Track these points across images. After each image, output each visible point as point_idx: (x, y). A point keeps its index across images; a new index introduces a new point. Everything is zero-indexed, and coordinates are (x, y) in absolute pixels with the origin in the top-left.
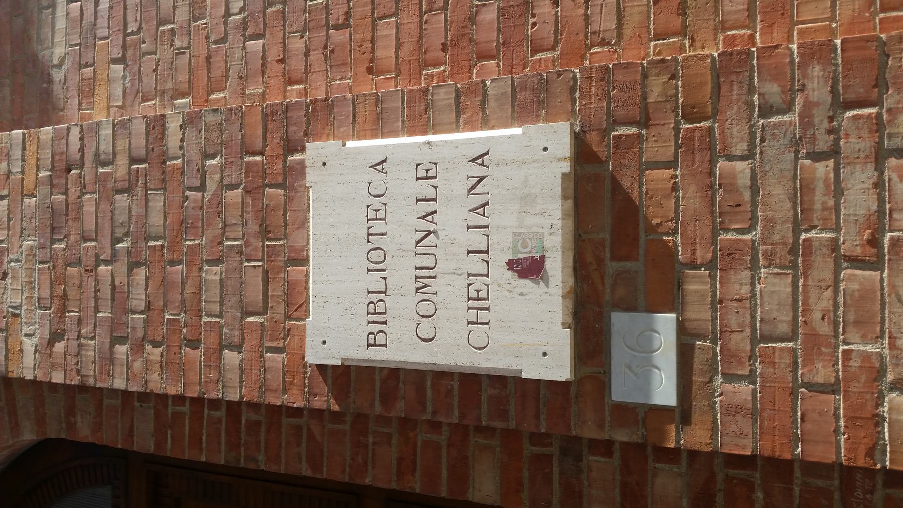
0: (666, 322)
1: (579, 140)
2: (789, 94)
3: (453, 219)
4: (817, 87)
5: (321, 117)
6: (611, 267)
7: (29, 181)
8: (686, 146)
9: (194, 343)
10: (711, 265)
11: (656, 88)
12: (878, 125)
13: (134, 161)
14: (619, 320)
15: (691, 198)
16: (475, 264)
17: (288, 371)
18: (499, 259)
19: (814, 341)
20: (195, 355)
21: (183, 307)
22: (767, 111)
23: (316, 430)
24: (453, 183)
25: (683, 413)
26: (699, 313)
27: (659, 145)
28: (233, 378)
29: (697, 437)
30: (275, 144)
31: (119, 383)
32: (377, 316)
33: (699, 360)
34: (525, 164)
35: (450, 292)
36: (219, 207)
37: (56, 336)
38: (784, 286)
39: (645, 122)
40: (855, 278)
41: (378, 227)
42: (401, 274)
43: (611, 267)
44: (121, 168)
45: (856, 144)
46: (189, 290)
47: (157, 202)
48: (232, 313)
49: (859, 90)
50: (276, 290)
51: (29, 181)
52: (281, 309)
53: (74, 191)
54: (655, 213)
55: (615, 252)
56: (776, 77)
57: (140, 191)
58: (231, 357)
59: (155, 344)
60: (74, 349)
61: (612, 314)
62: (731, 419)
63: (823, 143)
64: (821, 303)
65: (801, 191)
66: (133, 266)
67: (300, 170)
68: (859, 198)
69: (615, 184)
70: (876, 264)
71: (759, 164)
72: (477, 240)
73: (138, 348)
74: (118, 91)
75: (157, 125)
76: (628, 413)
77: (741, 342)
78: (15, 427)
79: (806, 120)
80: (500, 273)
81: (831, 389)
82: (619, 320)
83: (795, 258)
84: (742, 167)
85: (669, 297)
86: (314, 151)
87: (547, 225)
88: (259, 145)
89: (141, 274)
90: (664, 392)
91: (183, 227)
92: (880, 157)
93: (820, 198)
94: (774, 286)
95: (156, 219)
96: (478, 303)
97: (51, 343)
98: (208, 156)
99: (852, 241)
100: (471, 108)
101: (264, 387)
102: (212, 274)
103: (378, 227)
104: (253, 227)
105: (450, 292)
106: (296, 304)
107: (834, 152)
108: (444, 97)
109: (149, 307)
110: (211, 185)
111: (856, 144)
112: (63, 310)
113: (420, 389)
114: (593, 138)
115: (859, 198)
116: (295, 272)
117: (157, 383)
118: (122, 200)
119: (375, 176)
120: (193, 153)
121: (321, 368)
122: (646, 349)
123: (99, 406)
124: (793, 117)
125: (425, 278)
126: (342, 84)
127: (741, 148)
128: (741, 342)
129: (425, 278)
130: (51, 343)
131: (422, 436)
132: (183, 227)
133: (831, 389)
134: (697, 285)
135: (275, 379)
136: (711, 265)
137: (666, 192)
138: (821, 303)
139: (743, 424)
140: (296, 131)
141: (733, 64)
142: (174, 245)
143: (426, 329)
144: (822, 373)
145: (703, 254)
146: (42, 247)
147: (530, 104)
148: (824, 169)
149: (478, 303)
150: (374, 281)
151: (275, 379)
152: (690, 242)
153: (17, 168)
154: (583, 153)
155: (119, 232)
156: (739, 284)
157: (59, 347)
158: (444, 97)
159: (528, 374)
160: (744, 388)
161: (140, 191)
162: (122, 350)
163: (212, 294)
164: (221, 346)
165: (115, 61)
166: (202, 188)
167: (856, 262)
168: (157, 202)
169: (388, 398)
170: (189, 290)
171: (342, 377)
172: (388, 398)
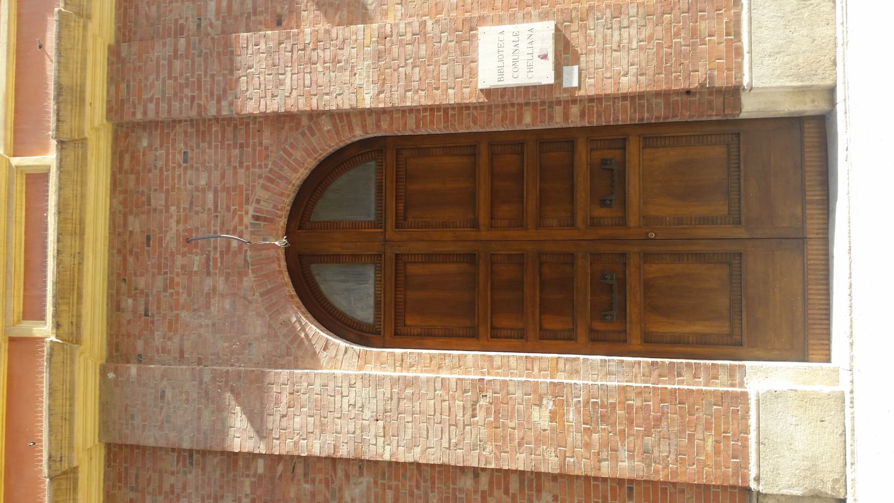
0: (576, 68)
1: (556, 26)
2: (603, 15)
3: (523, 46)
4: (608, 14)
5: (482, 20)
6: (563, 56)
7: (367, 41)
8: (581, 27)
9: (437, 89)
10: (586, 54)
11: (574, 14)
12: (620, 22)
13: (414, 35)
14: (565, 68)
15: (582, 39)
16: (530, 57)
17: (471, 93)
18: (536, 56)
19: (607, 68)
20: (438, 92)
21: (433, 78)
22: (598, 19)
23: (475, 113)
24: (523, 37)
25: (579, 88)
26: (583, 65)
27: (574, 27)
28: (452, 97)
29: (582, 93)
30: (466, 28)
31: (408, 104)
32: (501, 73)
33: (583, 75)
34: (543, 32)
35: (522, 65)
36: (446, 48)
37: (380, 93)
38: (601, 57)
39: (571, 22)
40: (615, 54)
41: (501, 49)
42: (508, 61)
43: (563, 56)
44: (409, 37)
45: (616, 26)
46: (435, 73)
47: (423, 47)
48: (451, 78)
49: (616, 15)
50: (466, 70)
51: (367, 41)
52: (468, 76)
53: (388, 45)
54: (573, 43)
55: (564, 52)
56: (600, 11)
57: (416, 44)
58: (451, 91)
59: (422, 90)
60: (388, 94)
61: (313, 266)
62: (590, 89)
63: (609, 26)
64: (608, 60)
65: (605, 37)
66: (414, 67)
67: (475, 36)
68: (616, 38)
69: (565, 37)
70: (619, 51)
71: (596, 30)
72: (530, 51)
73: (416, 92)
74: (400, 14)
75: (423, 24)
76: (566, 90)
77: (592, 70)
78: (351, 130)
79: (606, 21)
80: (536, 58)
81: (610, 78)
82: (565, 68)
83: (604, 50)
84: (593, 32)
85: (576, 61)
86: (481, 29)
87: (549, 47)
88: (461, 29)
89: (417, 70)
90: (575, 84)
91: (434, 54)
92: (620, 28)
93: (609, 38)
94: (599, 57)
95: (423, 52)
96: (530, 67)
97: (378, 94)
98: (442, 33)
99: (615, 47)
100: (527, 18)
101: (463, 98)
102: (444, 68)
103: (501, 49)
104: (458, 53)
105: (522, 65)
106: (473, 74)
107: (611, 28)
108: (520, 15)
109: (420, 79)
110: (443, 41)
111: (616, 26)
112: (383, 84)
113: (512, 92)
114: (559, 25)
115: (616, 38)
116: (473, 65)
117: (424, 102)
118: (409, 47)
119: (501, 36)
120: (437, 31)
121: (482, 90)
122: (571, 74)
123: (392, 118)
124: (603, 20)
125: (515, 63)
126: (485, 12)
127: (592, 27)
128: (592, 70)
129: (515, 63)
130: (378, 94)
131: (509, 110)
132: (434, 54)
133: (610, 78)
134: (583, 59)
135: (467, 96)
136: (586, 54)
137: (576, 38)
138: (608, 60)
139: (593, 88)
140: (473, 25)
141: (591, 9)
142: (430, 60)
143: (515, 75)
144: (609, 75)
145: (584, 52)
146: (373, 64)
147: (544, 16)
148: (609, 31)
149: (530, 67)
150: (500, 64)
151: (467, 96)
152: (581, 49)
153: (361, 37)
154: (557, 29)
155: (408, 57)
156: (592, 57)
157: (382, 96)
158: (520, 15)
159: (544, 83)
160: (592, 80)
161: (416, 44)
162: (409, 94)
163: (443, 75)
164: (447, 89)
165: (398, 4)
166: (440, 42)
167: (616, 51)
168: (423, 47)
169: (502, 96)
170: (435, 73)
171: (488, 92)
172: (502, 96)
